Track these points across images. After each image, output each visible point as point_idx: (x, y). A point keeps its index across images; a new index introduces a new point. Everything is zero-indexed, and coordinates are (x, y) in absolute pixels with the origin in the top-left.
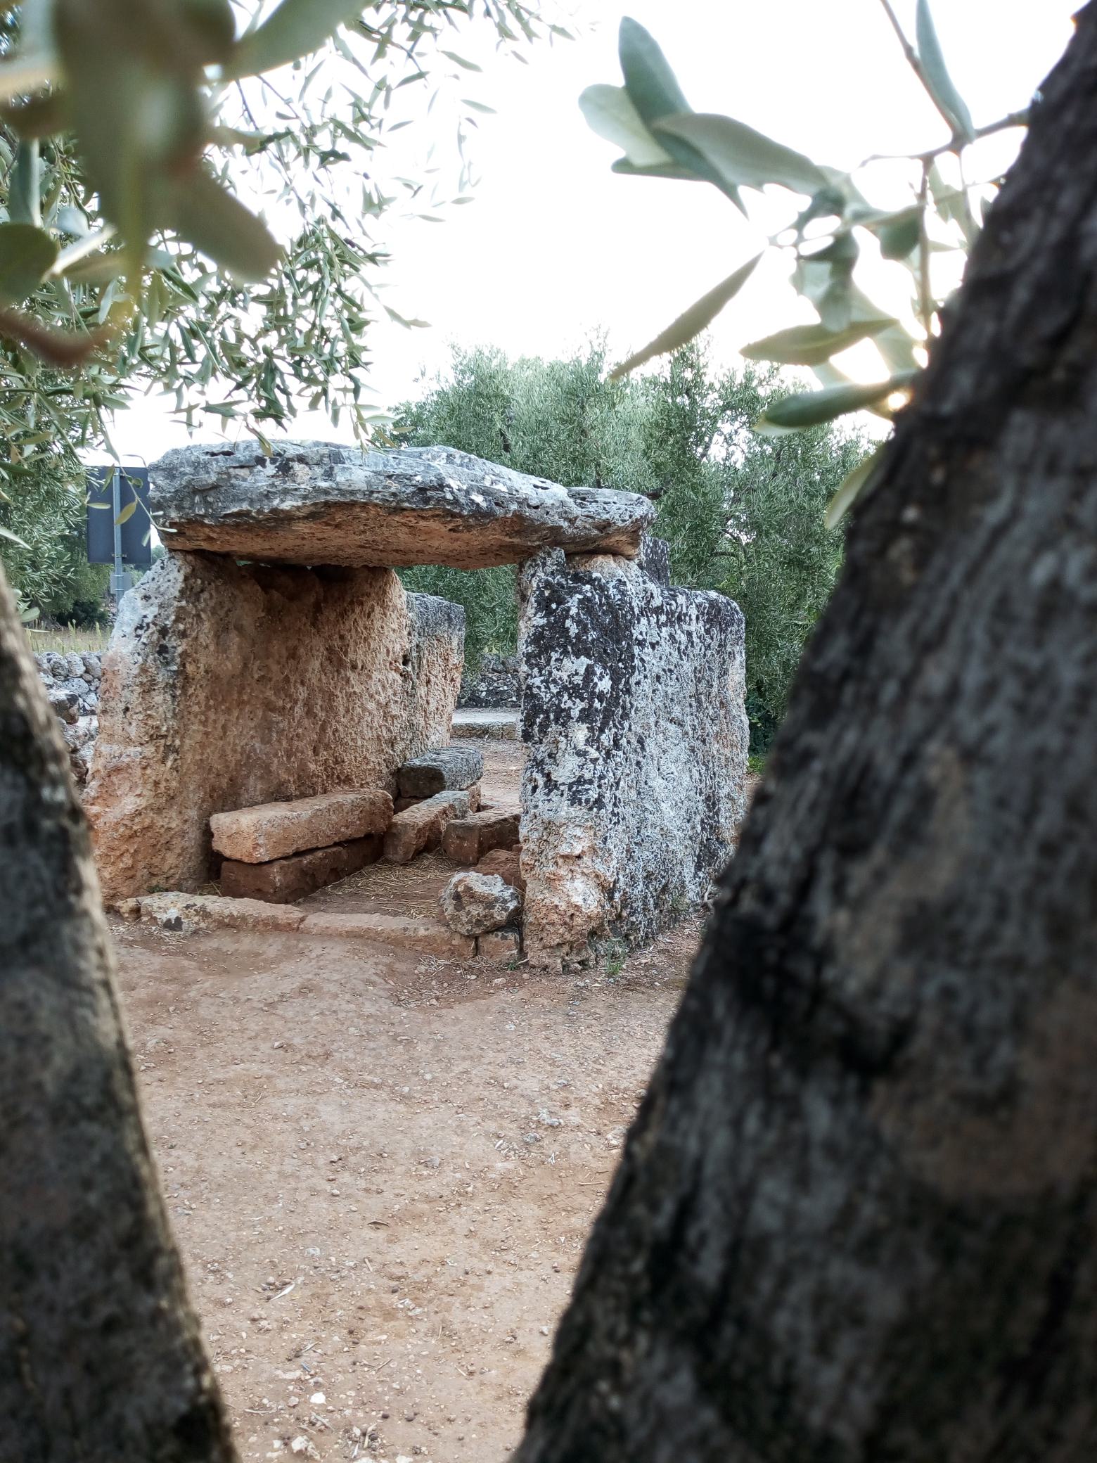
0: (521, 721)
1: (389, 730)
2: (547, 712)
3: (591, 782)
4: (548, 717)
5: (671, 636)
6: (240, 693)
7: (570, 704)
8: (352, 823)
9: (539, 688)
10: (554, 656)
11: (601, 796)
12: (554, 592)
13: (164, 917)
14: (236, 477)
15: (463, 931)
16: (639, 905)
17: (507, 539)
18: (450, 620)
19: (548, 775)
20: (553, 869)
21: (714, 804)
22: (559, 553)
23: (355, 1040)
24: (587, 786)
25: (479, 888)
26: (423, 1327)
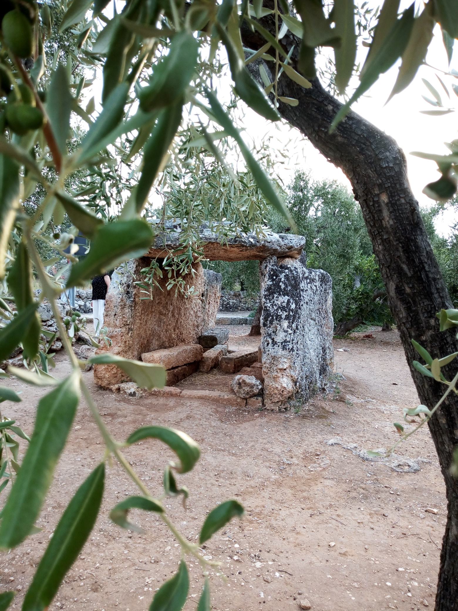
1: (197, 322)
2: (272, 316)
3: (289, 342)
4: (273, 318)
5: (311, 287)
6: (152, 308)
7: (281, 313)
8: (190, 357)
10: (275, 296)
11: (293, 347)
12: (274, 272)
13: (129, 392)
15: (242, 397)
16: (303, 387)
17: (258, 253)
18: (217, 279)
19: (273, 339)
20: (276, 374)
21: (325, 350)
22: (275, 258)
23: (211, 435)
24: (288, 343)
25: (248, 381)
26: (264, 526)
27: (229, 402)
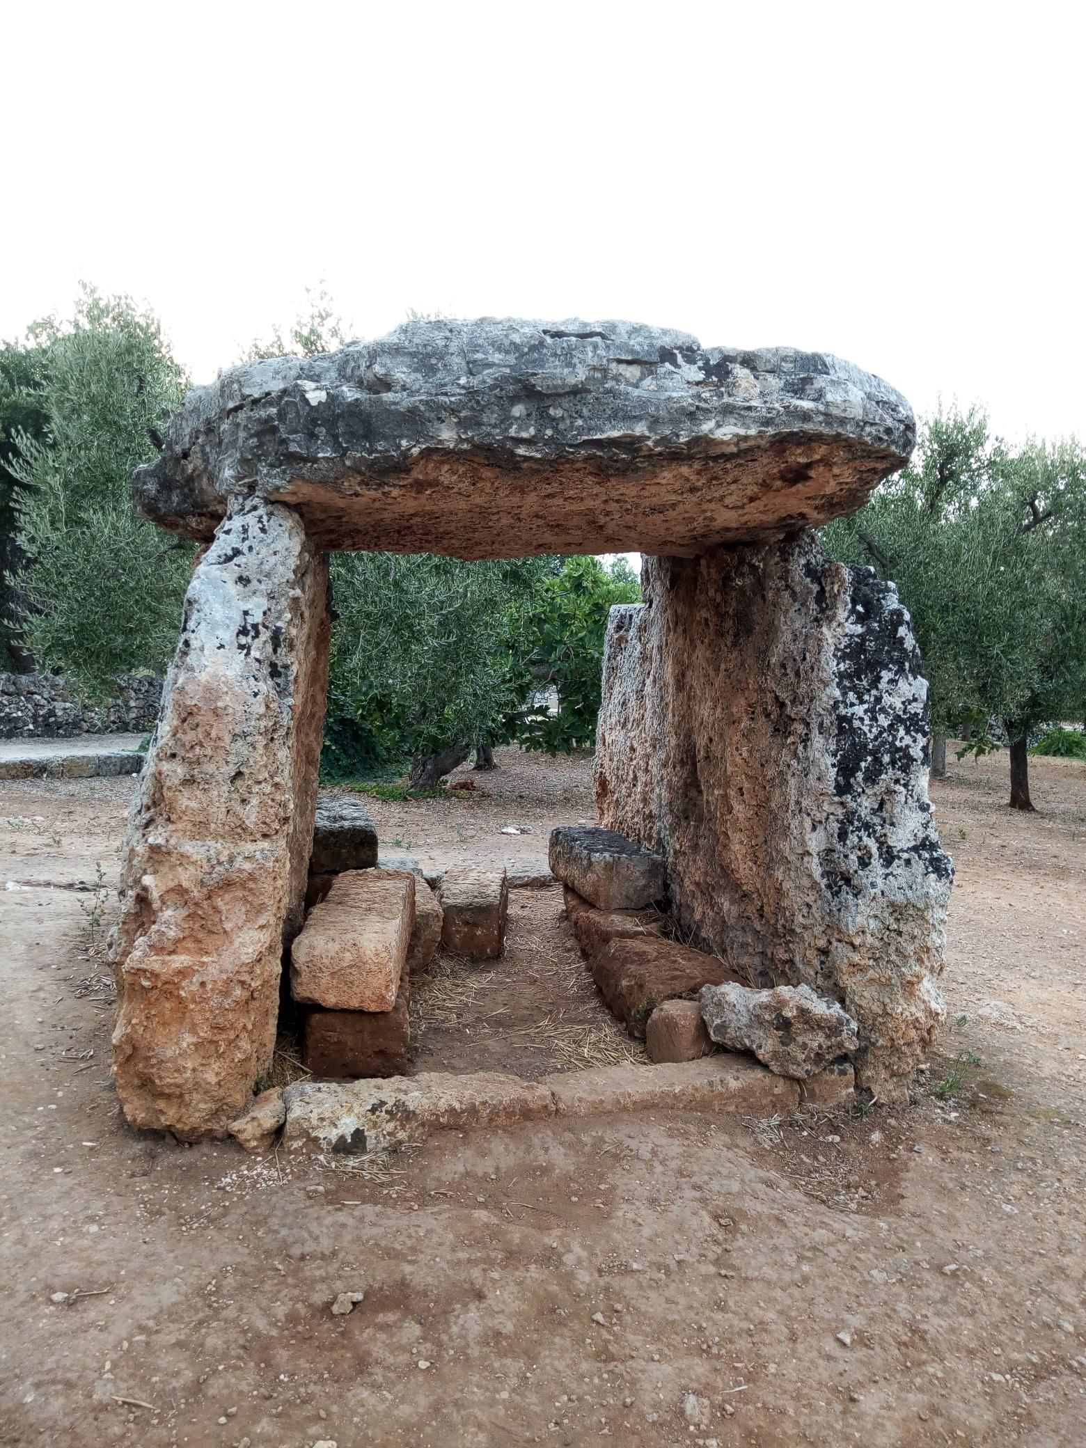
0: (833, 766)
2: (874, 753)
4: (877, 760)
9: (862, 719)
13: (334, 1134)
14: (616, 378)
27: (749, 1103)
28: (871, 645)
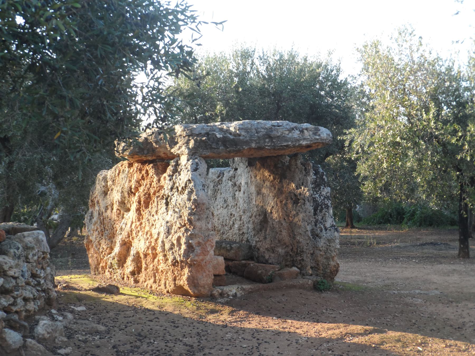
4: (322, 207)
7: (327, 202)
28: (318, 180)
